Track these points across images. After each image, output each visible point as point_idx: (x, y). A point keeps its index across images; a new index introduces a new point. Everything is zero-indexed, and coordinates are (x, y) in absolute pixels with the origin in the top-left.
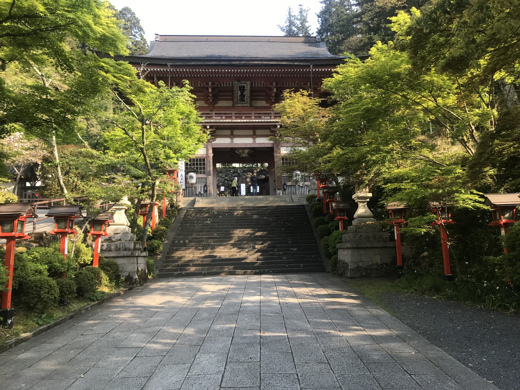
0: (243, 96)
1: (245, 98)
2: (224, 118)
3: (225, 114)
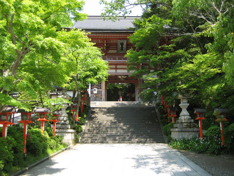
0: (122, 47)
1: (124, 49)
2: (112, 59)
3: (113, 57)
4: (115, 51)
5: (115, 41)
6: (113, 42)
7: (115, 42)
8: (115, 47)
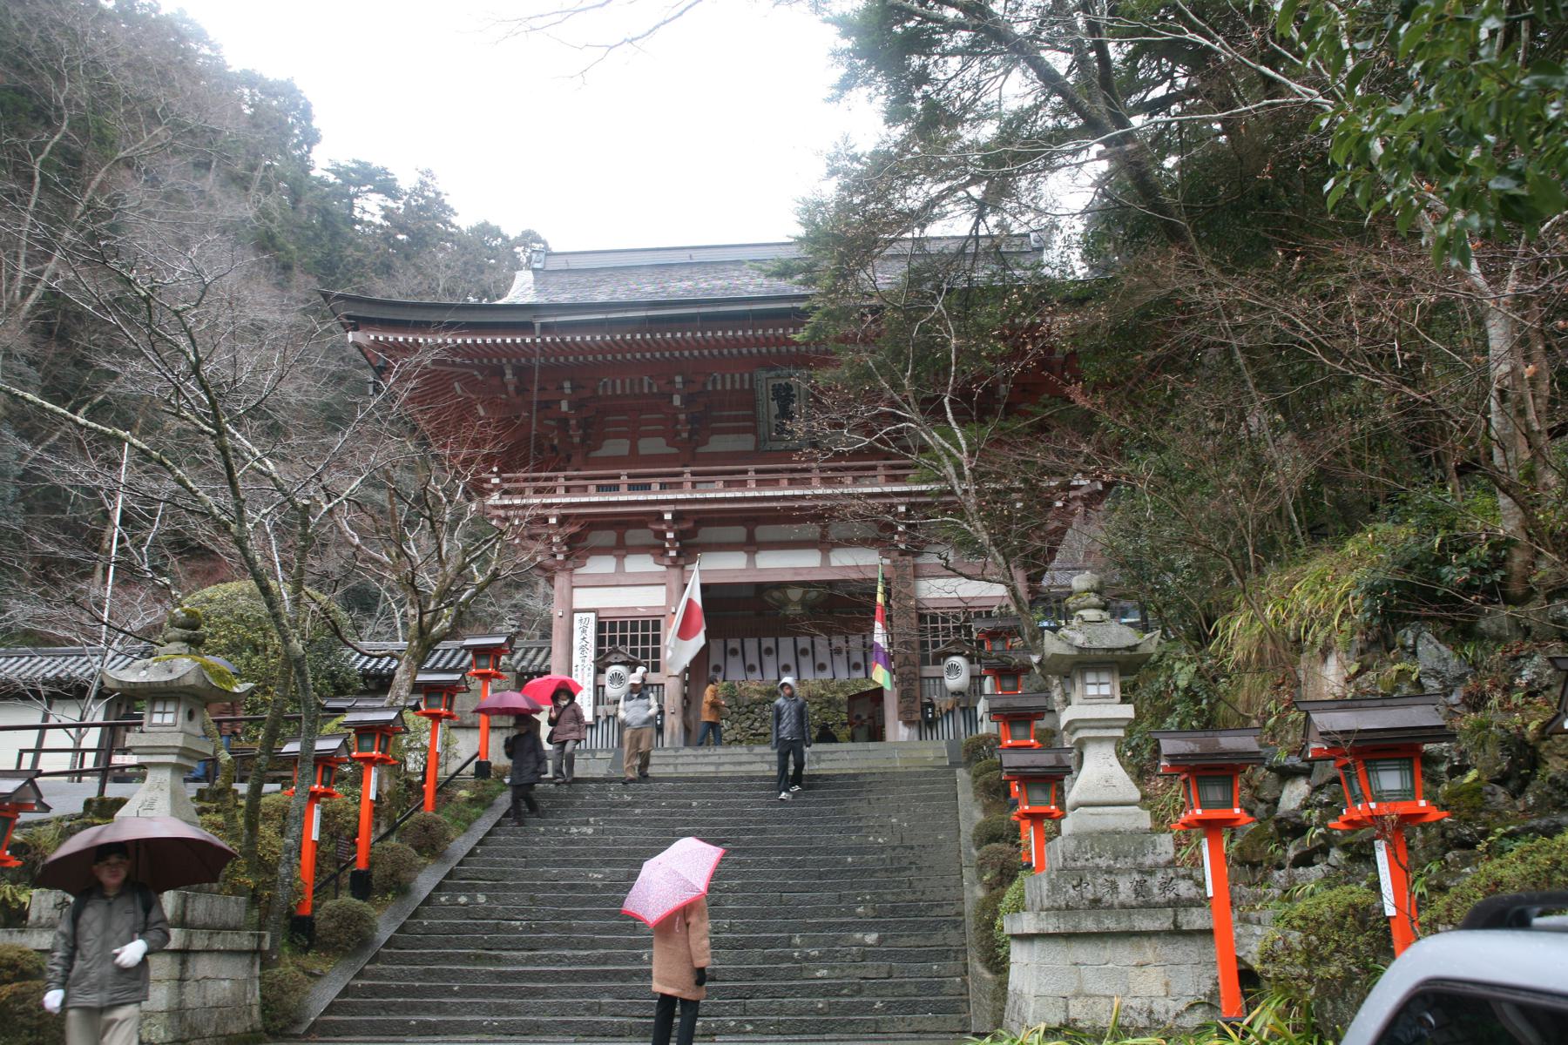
4: (746, 443)
5: (737, 376)
6: (728, 387)
7: (737, 386)
8: (745, 418)
